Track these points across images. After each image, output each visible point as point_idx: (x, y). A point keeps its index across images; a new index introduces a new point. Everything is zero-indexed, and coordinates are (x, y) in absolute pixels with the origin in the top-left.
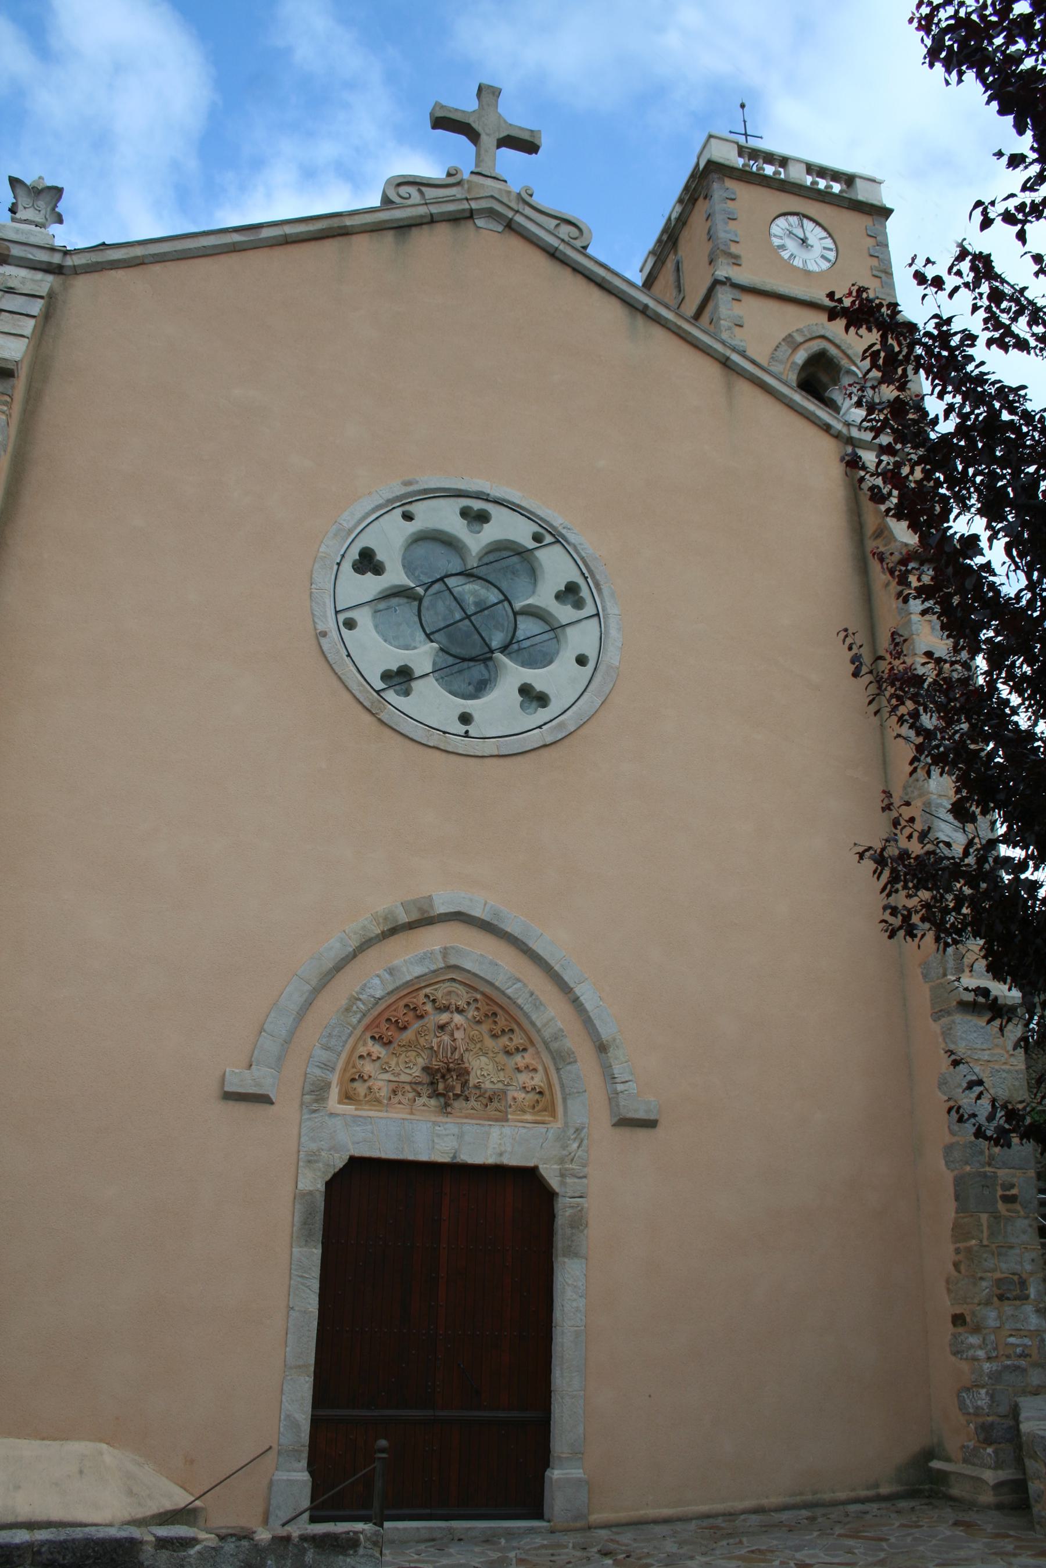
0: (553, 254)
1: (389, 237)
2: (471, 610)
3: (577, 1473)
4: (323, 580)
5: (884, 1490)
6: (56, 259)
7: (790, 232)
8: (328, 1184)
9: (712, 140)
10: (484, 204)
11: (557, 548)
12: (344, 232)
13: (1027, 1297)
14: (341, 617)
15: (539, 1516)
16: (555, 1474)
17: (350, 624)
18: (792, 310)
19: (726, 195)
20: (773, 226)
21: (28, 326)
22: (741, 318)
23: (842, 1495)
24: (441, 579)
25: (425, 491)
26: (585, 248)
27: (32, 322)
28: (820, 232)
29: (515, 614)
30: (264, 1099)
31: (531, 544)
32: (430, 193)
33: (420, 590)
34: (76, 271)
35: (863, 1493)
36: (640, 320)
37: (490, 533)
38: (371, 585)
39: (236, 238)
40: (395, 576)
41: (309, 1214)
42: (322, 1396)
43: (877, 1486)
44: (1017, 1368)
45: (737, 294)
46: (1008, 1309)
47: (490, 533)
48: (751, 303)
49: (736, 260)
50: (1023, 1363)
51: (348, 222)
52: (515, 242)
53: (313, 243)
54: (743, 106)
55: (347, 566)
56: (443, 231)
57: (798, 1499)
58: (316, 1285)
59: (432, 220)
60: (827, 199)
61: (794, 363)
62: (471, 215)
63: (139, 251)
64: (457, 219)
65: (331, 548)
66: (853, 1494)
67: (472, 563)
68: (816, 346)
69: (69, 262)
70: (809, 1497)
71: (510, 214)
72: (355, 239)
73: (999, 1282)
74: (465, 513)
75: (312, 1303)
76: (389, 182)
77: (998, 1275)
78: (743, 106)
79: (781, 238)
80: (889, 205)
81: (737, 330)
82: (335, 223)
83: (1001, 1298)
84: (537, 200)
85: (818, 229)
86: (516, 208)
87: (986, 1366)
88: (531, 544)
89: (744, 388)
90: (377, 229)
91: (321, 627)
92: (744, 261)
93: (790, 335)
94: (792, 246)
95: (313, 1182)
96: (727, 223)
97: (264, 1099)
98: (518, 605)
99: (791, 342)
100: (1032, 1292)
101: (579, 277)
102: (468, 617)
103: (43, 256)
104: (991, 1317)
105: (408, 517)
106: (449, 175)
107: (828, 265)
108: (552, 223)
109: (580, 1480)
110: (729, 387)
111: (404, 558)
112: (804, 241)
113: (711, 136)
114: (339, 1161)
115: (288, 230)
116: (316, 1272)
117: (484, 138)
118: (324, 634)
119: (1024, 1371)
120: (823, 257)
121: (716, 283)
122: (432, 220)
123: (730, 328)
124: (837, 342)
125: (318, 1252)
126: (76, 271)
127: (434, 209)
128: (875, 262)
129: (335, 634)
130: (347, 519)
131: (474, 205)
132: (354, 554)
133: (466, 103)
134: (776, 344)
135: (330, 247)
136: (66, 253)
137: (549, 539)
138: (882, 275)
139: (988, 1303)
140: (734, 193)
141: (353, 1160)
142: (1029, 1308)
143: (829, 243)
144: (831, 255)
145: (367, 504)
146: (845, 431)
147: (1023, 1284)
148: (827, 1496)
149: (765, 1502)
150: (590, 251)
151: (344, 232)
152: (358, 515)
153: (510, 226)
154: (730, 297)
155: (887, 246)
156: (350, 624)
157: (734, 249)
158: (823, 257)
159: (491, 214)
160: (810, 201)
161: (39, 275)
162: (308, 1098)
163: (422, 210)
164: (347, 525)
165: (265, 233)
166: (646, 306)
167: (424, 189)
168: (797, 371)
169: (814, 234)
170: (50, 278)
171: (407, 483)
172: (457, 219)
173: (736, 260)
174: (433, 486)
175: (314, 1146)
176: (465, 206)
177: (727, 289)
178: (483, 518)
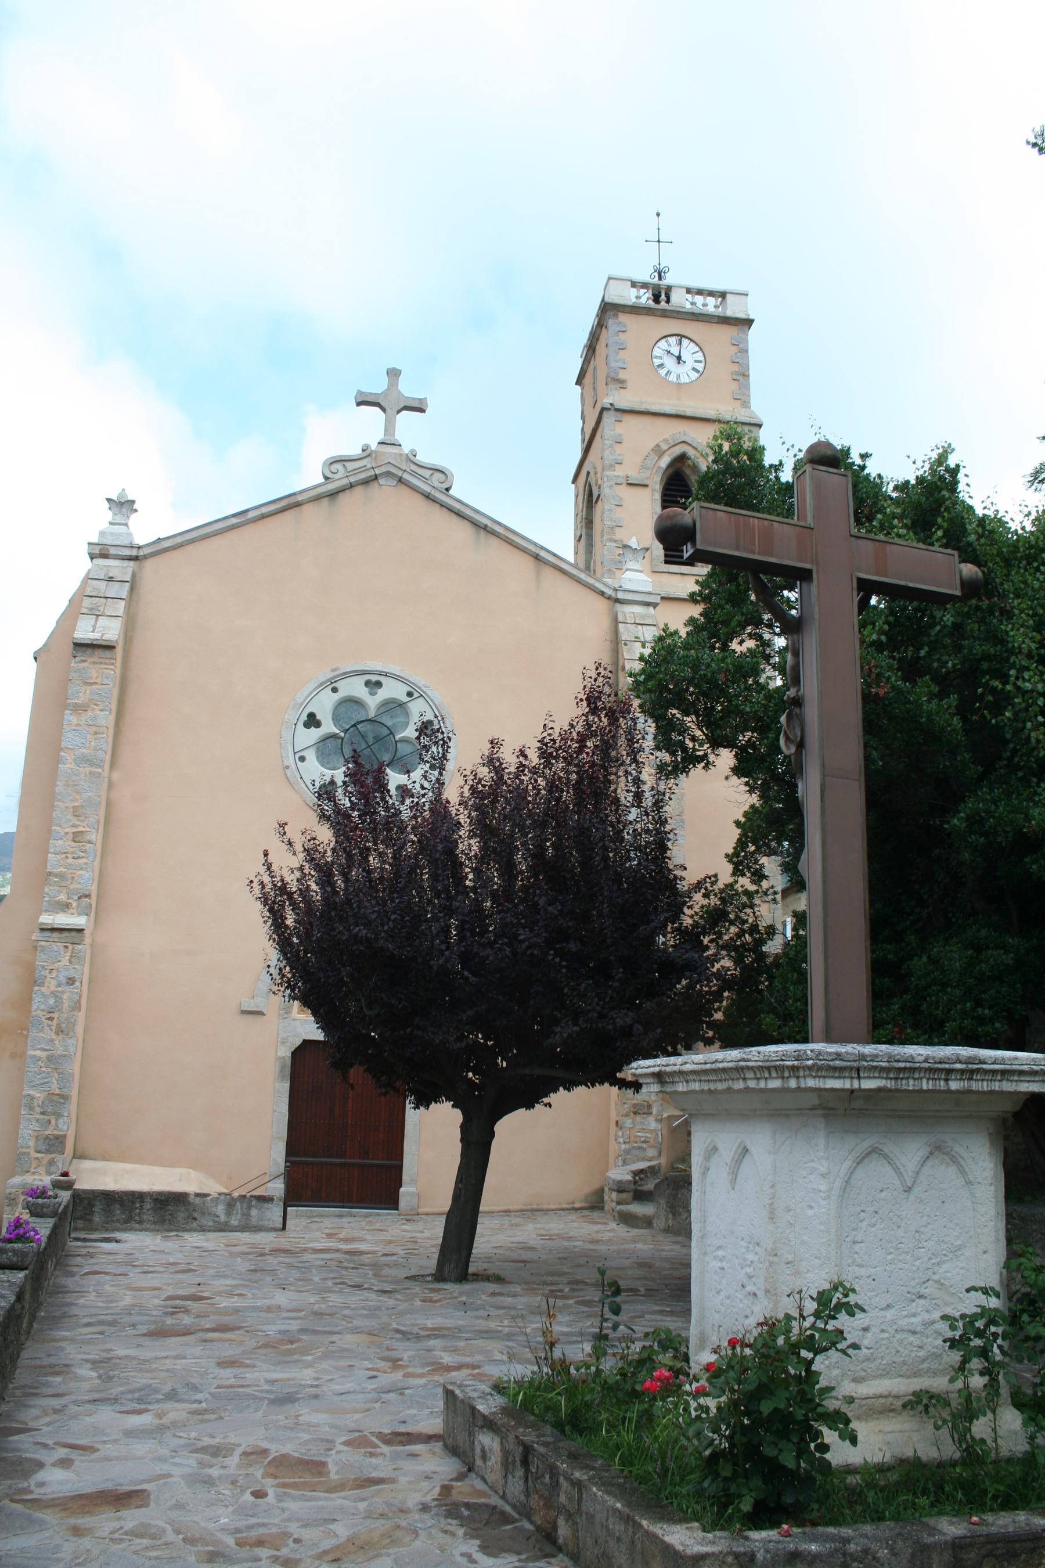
0: (428, 497)
1: (325, 501)
2: (371, 741)
3: (413, 1189)
4: (287, 736)
5: (577, 1205)
6: (134, 553)
7: (669, 352)
8: (293, 1053)
9: (611, 281)
10: (384, 469)
11: (421, 699)
12: (298, 505)
13: (651, 1113)
14: (297, 756)
15: (397, 1209)
16: (402, 1190)
17: (302, 759)
18: (661, 422)
19: (618, 329)
20: (656, 349)
21: (120, 607)
22: (621, 435)
23: (553, 1207)
24: (354, 725)
25: (345, 673)
26: (448, 489)
27: (123, 603)
28: (693, 347)
29: (396, 742)
30: (260, 1013)
31: (405, 699)
32: (351, 466)
33: (342, 734)
34: (145, 557)
35: (565, 1206)
36: (482, 532)
37: (383, 694)
38: (314, 734)
39: (234, 521)
40: (329, 727)
41: (283, 1067)
42: (291, 1150)
43: (573, 1203)
44: (640, 1148)
45: (619, 414)
46: (639, 1118)
47: (383, 694)
48: (630, 420)
49: (621, 384)
50: (644, 1145)
51: (300, 498)
52: (404, 490)
53: (280, 515)
54: (658, 215)
55: (300, 724)
56: (359, 491)
57: (529, 1207)
58: (287, 1101)
59: (351, 486)
60: (700, 318)
61: (659, 467)
62: (376, 477)
63: (179, 540)
64: (366, 482)
65: (291, 716)
66: (559, 1207)
67: (372, 714)
68: (677, 451)
69: (141, 553)
70: (535, 1207)
71: (400, 473)
72: (304, 507)
73: (635, 1105)
74: (368, 683)
75: (284, 1108)
76: (324, 463)
77: (635, 1102)
78: (658, 215)
79: (661, 358)
80: (751, 317)
81: (617, 446)
82: (292, 500)
83: (635, 1113)
84: (421, 458)
85: (692, 345)
86: (404, 468)
87: (623, 1146)
88: (405, 699)
89: (548, 572)
90: (317, 498)
91: (286, 763)
92: (629, 385)
93: (658, 446)
94: (670, 363)
95: (286, 1052)
96: (617, 354)
97: (260, 1013)
98: (397, 737)
99: (658, 451)
100: (654, 1111)
101: (444, 510)
102: (369, 746)
103: (127, 552)
104: (628, 1122)
105: (335, 690)
106: (363, 451)
107: (697, 375)
108: (427, 473)
109: (413, 1193)
110: (538, 573)
111: (333, 714)
112: (679, 358)
113: (610, 278)
114: (298, 1042)
115: (264, 510)
116: (287, 1094)
117: (388, 410)
118: (287, 767)
119: (644, 1149)
120: (694, 369)
121: (603, 409)
122: (351, 486)
123: (611, 446)
124: (695, 445)
125: (287, 1085)
126: (145, 557)
127: (352, 479)
128: (735, 368)
129: (293, 767)
130: (300, 698)
131: (378, 471)
132: (304, 717)
133: (378, 386)
134: (646, 453)
135: (289, 515)
136: (139, 548)
137: (416, 695)
138: (740, 378)
139: (627, 1115)
140: (625, 326)
141: (305, 1041)
142: (651, 1119)
143: (699, 356)
144: (700, 367)
145: (311, 686)
146: (613, 595)
147: (649, 1106)
148: (545, 1207)
149: (511, 1208)
150: (451, 492)
151: (298, 505)
152: (306, 694)
153: (400, 480)
154: (613, 419)
155: (747, 351)
156: (302, 759)
157: (622, 375)
158: (694, 369)
159: (388, 474)
160: (687, 322)
161: (126, 563)
162: (282, 1012)
163: (345, 482)
164: (299, 701)
165: (251, 515)
166: (486, 526)
167: (346, 464)
168: (660, 474)
169: (688, 350)
170: (132, 563)
171: (333, 670)
172: (366, 482)
173: (621, 384)
174: (348, 670)
175: (285, 1035)
176: (372, 473)
177: (612, 412)
178: (379, 684)
